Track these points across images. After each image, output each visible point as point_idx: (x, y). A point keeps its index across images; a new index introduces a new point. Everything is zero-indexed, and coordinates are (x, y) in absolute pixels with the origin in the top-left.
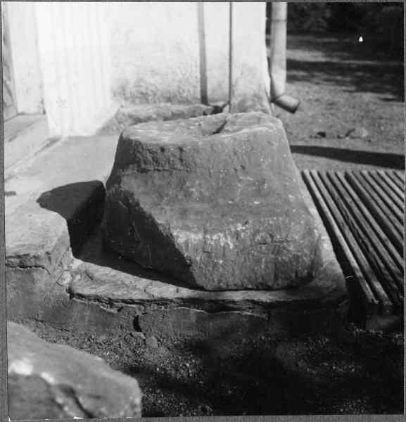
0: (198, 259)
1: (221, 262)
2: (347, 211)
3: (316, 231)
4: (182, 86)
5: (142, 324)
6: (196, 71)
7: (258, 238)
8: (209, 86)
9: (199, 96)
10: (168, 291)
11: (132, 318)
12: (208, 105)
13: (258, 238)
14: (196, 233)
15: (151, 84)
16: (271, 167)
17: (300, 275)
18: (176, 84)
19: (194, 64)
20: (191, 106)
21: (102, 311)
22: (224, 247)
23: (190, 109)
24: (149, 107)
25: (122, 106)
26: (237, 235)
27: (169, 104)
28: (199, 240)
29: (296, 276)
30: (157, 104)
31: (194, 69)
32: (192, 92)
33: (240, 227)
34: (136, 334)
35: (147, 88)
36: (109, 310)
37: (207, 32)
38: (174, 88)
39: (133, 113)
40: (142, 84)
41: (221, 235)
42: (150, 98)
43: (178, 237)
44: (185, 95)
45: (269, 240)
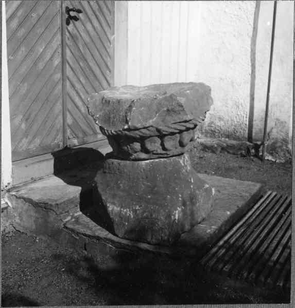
0: (117, 220)
1: (127, 224)
3: (172, 217)
4: (236, 128)
5: (87, 247)
6: (246, 121)
7: (145, 215)
8: (254, 131)
9: (246, 136)
10: (103, 233)
11: (84, 243)
12: (251, 142)
13: (145, 215)
14: (117, 207)
15: (218, 126)
17: (163, 239)
18: (233, 127)
19: (245, 116)
20: (240, 142)
21: (73, 237)
22: (129, 216)
23: (239, 144)
24: (215, 140)
26: (135, 211)
27: (227, 139)
28: (118, 211)
29: (162, 238)
30: (220, 139)
31: (245, 119)
32: (242, 134)
34: (84, 251)
35: (215, 128)
36: (76, 237)
37: (256, 96)
38: (231, 129)
39: (204, 143)
40: (213, 125)
41: (128, 210)
42: (216, 134)
43: (109, 207)
44: (238, 134)
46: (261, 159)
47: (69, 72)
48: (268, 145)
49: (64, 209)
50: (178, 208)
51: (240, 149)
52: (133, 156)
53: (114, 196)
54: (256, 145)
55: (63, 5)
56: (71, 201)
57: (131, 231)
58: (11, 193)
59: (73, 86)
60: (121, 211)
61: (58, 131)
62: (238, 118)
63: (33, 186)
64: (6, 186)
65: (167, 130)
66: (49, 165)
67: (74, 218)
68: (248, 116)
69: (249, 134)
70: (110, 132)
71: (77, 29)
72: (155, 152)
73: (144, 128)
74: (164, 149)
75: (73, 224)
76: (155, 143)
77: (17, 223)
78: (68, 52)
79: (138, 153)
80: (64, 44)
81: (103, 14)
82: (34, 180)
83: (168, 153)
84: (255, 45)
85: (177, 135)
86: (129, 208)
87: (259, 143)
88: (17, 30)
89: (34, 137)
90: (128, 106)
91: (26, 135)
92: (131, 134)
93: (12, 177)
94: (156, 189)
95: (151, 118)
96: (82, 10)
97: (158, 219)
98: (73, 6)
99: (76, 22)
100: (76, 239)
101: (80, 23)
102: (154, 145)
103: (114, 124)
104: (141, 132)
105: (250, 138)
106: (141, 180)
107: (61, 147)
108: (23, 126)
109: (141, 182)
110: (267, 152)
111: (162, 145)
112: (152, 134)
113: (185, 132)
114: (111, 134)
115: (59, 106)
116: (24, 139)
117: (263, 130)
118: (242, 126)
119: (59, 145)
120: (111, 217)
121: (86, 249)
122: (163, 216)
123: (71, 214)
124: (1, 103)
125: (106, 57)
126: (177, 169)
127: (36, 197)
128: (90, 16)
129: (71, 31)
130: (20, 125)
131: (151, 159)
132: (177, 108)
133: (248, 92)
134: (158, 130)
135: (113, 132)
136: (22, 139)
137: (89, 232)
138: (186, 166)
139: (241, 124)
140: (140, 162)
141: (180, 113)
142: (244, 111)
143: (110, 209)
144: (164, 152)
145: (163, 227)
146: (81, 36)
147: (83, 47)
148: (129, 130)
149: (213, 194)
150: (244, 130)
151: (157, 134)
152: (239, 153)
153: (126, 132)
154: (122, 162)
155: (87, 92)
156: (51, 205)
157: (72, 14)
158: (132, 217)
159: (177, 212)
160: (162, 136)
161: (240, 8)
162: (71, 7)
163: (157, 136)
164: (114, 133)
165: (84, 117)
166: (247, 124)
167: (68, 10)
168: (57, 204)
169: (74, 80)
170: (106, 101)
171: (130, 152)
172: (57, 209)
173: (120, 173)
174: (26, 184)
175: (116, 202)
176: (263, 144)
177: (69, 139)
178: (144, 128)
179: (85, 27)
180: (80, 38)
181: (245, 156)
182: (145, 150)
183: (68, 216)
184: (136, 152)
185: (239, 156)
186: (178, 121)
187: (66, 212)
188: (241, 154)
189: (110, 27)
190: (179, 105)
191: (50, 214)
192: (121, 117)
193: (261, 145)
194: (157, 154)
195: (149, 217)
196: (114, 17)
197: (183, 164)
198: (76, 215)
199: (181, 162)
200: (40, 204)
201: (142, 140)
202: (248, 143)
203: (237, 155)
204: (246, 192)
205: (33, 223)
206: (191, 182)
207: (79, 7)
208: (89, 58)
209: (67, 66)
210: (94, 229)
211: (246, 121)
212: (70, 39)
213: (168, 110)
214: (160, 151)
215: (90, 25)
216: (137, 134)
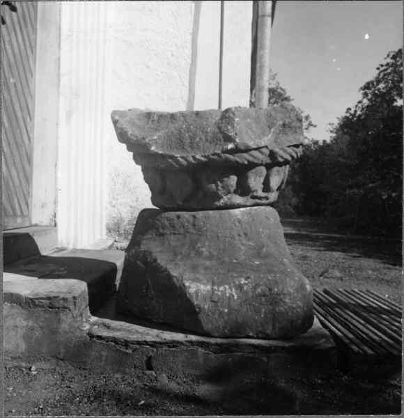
0: (206, 307)
5: (154, 363)
7: (259, 290)
22: (229, 298)
25: (116, 241)
26: (240, 287)
28: (208, 291)
33: (243, 281)
41: (227, 287)
52: (222, 201)
53: (194, 268)
86: (229, 284)
94: (264, 250)
97: (284, 294)
100: (127, 353)
104: (252, 156)
109: (237, 242)
114: (193, 162)
122: (292, 287)
132: (296, 124)
135: (198, 157)
140: (231, 211)
144: (264, 195)
153: (228, 155)
154: (200, 214)
156: (65, 299)
158: (236, 297)
161: (168, 64)
164: (203, 159)
173: (199, 230)
175: (201, 278)
182: (243, 189)
190: (298, 119)
191: (63, 316)
195: (267, 293)
201: (242, 171)
213: (284, 125)
214: (260, 193)
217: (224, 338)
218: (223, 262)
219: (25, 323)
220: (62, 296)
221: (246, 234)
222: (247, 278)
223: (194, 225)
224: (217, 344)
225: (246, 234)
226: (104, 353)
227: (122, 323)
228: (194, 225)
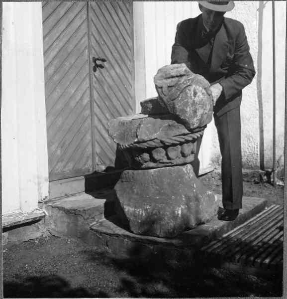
2: (258, 215)
3: (176, 212)
5: (109, 244)
9: (259, 164)
10: (121, 231)
11: (106, 241)
14: (132, 208)
16: (169, 184)
19: (256, 147)
20: (253, 171)
23: (252, 172)
25: (215, 169)
26: (146, 210)
31: (256, 149)
33: (148, 207)
41: (141, 209)
44: (250, 164)
45: (158, 214)
46: (273, 184)
47: (96, 110)
48: (278, 172)
49: (90, 215)
50: (182, 206)
51: (254, 177)
52: (144, 166)
54: (268, 172)
55: (91, 57)
56: (96, 209)
57: (143, 224)
58: (48, 204)
59: (100, 120)
60: (135, 211)
61: (88, 157)
62: (249, 149)
63: (67, 199)
64: (44, 199)
65: (169, 142)
66: (81, 184)
67: (100, 222)
68: (259, 147)
69: (261, 162)
70: (124, 146)
71: (102, 75)
72: (161, 161)
73: (151, 140)
74: (169, 158)
75: (98, 227)
76: (160, 153)
77: (52, 229)
78: (95, 93)
79: (147, 163)
80: (92, 87)
81: (125, 63)
82: (67, 196)
83: (172, 161)
84: (260, 84)
85: (179, 146)
86: (141, 208)
87: (270, 170)
88: (53, 75)
89: (67, 163)
90: (138, 124)
91: (61, 159)
92: (142, 146)
93: (49, 192)
95: (156, 132)
96: (106, 59)
98: (98, 56)
99: (101, 69)
100: (100, 238)
101: (106, 71)
102: (160, 155)
103: (127, 139)
104: (148, 144)
105: (262, 167)
106: (151, 184)
107: (91, 171)
108: (59, 152)
110: (277, 178)
111: (167, 155)
112: (157, 145)
113: (185, 144)
115: (89, 137)
116: (60, 163)
117: (272, 159)
118: (254, 156)
119: (89, 169)
120: (128, 216)
121: (107, 246)
123: (97, 220)
124: (33, 1)
125: (128, 98)
126: (181, 176)
127: (68, 206)
128: (113, 64)
129: (97, 76)
130: (56, 151)
131: (159, 167)
133: (257, 126)
134: (162, 142)
136: (58, 162)
137: (110, 232)
138: (189, 174)
139: (252, 154)
141: (178, 128)
142: (254, 143)
143: (126, 210)
144: (168, 161)
145: (169, 221)
146: (106, 80)
147: (108, 89)
148: (138, 142)
149: (216, 200)
150: (256, 159)
151: (161, 145)
152: (253, 180)
153: (137, 145)
154: (136, 172)
155: (108, 119)
156: (79, 211)
157: (98, 62)
158: (144, 215)
159: (180, 208)
160: (166, 147)
162: (96, 57)
163: (161, 147)
165: (110, 147)
166: (259, 153)
167: (95, 60)
168: (85, 210)
169: (101, 117)
170: (122, 123)
171: (141, 162)
172: (84, 214)
174: (60, 198)
176: (273, 171)
177: (97, 165)
178: (151, 140)
179: (110, 74)
180: (105, 81)
181: (258, 183)
182: (153, 160)
183: (94, 221)
184: (146, 162)
185: (253, 183)
186: (178, 134)
187: (92, 218)
188: (254, 181)
189: (131, 74)
191: (79, 219)
192: (133, 134)
193: (272, 172)
194: (163, 163)
196: (134, 65)
197: (186, 172)
198: (100, 221)
199: (184, 169)
200: (70, 211)
201: (149, 150)
202: (260, 171)
203: (251, 182)
204: (251, 204)
205: (65, 228)
206: (194, 187)
207: (103, 57)
208: (114, 99)
209: (95, 104)
210: (114, 230)
211: (257, 151)
212: (97, 82)
214: (165, 160)
215: (113, 71)
216: (145, 145)
217: (139, 234)
218: (143, 197)
219: (67, 220)
220: (78, 209)
221: (155, 182)
222: (150, 206)
223: (133, 177)
224: (134, 238)
225: (155, 182)
226: (92, 237)
227: (111, 223)
228: (133, 177)
